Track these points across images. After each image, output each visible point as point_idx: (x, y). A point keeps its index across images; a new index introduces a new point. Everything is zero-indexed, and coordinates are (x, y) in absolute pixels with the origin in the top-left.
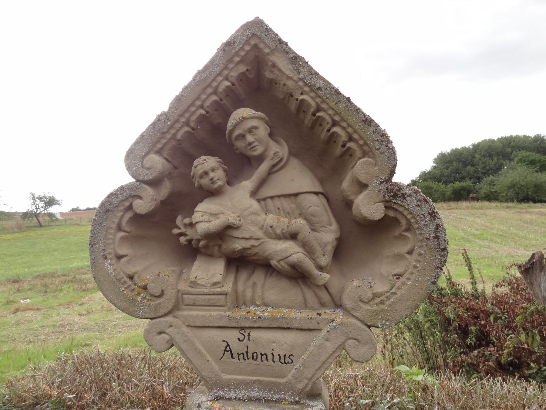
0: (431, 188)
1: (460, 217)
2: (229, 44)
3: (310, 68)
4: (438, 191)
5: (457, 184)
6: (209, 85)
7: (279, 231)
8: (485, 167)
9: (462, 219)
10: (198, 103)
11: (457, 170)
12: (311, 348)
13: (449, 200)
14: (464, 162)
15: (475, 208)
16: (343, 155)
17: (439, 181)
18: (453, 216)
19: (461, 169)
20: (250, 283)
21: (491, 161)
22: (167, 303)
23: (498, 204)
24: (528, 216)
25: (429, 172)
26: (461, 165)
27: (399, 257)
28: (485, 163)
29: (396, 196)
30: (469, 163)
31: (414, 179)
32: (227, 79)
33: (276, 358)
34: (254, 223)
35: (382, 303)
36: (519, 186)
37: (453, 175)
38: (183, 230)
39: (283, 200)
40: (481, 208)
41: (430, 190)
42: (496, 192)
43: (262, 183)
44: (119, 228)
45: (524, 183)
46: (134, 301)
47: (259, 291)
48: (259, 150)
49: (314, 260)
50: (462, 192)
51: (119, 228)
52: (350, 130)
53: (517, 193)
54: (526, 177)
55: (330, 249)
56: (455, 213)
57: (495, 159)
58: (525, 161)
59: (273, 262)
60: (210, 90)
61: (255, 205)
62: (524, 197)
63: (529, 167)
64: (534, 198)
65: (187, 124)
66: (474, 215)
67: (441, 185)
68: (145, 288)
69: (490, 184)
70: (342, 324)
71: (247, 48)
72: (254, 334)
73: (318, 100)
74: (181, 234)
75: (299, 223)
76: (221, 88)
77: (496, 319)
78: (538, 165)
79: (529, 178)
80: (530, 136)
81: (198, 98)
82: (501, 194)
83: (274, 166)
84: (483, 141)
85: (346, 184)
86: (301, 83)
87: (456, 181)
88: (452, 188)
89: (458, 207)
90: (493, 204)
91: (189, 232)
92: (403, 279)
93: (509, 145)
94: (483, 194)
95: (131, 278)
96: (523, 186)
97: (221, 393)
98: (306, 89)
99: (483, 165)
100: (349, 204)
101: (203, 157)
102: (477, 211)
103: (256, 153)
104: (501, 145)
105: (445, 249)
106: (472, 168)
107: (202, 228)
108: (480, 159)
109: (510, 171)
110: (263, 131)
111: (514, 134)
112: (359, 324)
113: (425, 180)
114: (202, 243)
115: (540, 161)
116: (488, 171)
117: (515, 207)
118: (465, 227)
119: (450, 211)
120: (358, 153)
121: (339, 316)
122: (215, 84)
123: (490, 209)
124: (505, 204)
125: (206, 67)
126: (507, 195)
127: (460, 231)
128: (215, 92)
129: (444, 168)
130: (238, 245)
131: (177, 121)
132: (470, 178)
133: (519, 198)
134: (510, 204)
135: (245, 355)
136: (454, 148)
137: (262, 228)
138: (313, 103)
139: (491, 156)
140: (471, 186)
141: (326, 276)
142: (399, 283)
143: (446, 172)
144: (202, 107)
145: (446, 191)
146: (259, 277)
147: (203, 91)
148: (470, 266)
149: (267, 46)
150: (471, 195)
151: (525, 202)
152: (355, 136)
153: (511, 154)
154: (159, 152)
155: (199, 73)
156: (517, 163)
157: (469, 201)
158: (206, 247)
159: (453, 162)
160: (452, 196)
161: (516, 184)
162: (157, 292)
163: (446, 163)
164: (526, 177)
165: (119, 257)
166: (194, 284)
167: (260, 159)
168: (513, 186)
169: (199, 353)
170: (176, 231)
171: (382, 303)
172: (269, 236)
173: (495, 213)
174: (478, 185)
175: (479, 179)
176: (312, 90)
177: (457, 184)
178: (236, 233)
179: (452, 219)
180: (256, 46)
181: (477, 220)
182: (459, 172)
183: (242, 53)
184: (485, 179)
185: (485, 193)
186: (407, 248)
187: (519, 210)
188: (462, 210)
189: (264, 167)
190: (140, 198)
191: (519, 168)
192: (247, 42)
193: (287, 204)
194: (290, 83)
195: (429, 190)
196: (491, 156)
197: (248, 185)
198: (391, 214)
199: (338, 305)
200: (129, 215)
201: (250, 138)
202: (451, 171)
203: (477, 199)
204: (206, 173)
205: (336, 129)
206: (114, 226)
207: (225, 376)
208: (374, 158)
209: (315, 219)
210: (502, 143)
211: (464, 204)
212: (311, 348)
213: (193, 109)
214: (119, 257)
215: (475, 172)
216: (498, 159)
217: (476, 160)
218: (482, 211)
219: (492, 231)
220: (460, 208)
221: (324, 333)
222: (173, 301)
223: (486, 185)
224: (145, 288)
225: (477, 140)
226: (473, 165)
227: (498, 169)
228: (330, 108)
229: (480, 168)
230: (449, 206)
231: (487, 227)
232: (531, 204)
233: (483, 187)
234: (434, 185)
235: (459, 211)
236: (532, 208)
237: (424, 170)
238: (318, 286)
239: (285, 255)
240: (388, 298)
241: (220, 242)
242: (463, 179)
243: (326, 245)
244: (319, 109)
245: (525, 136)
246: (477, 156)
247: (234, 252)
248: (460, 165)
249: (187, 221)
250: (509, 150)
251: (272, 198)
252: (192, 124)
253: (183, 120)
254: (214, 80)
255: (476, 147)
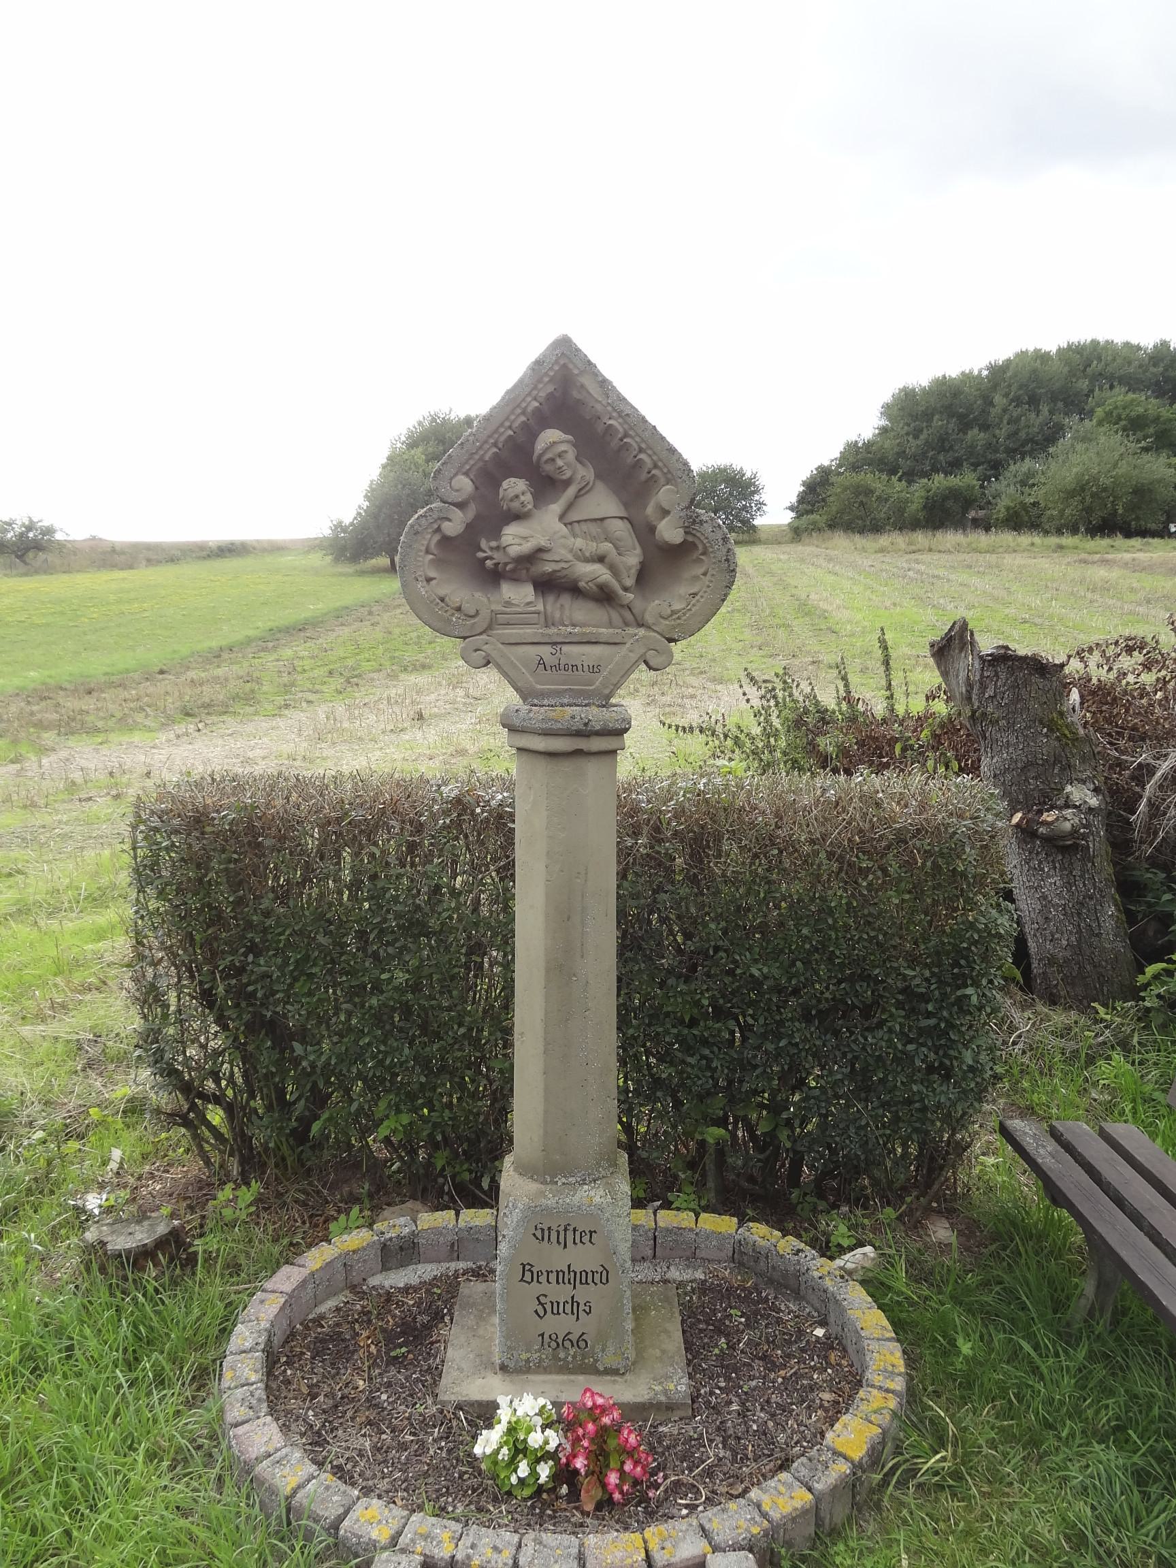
0: (869, 492)
1: (936, 573)
2: (538, 363)
3: (619, 395)
4: (887, 500)
5: (940, 481)
6: (518, 406)
7: (588, 554)
8: (1016, 433)
9: (938, 577)
10: (507, 424)
11: (942, 440)
12: (617, 659)
13: (914, 525)
14: (961, 417)
15: (976, 550)
16: (647, 481)
17: (893, 472)
18: (918, 572)
19: (954, 437)
20: (558, 605)
21: (1033, 415)
22: (481, 622)
23: (1037, 540)
24: (1101, 573)
25: (868, 445)
26: (953, 425)
27: (696, 578)
28: (1018, 420)
29: (694, 522)
30: (975, 419)
31: (826, 463)
32: (535, 399)
33: (586, 668)
34: (564, 546)
35: (679, 618)
36: (1094, 489)
37: (931, 454)
38: (489, 553)
39: (590, 524)
40: (992, 550)
41: (866, 495)
42: (1034, 504)
43: (570, 506)
44: (428, 552)
45: (1108, 482)
46: (449, 621)
47: (567, 613)
48: (568, 474)
49: (619, 582)
50: (949, 504)
51: (428, 552)
52: (655, 458)
53: (1089, 510)
54: (1115, 466)
55: (634, 572)
56: (924, 563)
57: (1045, 409)
58: (1120, 419)
59: (582, 584)
60: (519, 411)
61: (565, 530)
62: (1103, 519)
63: (1128, 436)
64: (1130, 525)
65: (495, 445)
66: (970, 567)
67: (897, 484)
68: (459, 609)
69: (1023, 483)
70: (644, 637)
71: (556, 368)
72: (565, 648)
73: (626, 426)
74: (487, 558)
75: (607, 547)
76: (530, 409)
77: (904, 750)
78: (1151, 430)
79: (1123, 468)
80: (1142, 345)
81: (507, 419)
82: (1049, 512)
83: (580, 490)
84: (1017, 355)
85: (650, 510)
86: (609, 408)
87: (937, 471)
88: (923, 494)
89: (933, 547)
90: (1025, 539)
91: (496, 555)
92: (698, 597)
93: (1084, 370)
94: (1003, 510)
95: (442, 600)
96: (1105, 490)
97: (536, 701)
98: (615, 414)
99: (1013, 428)
100: (652, 529)
101: (513, 480)
102: (981, 557)
103: (564, 477)
104: (1066, 370)
105: (734, 570)
106: (982, 434)
107: (514, 551)
108: (1005, 411)
109: (1080, 447)
110: (571, 455)
111: (1102, 338)
112: (659, 637)
113: (855, 468)
114: (508, 568)
115: (1157, 419)
116: (1023, 445)
117: (1076, 548)
118: (942, 601)
119: (913, 556)
120: (662, 481)
121: (642, 632)
122: (524, 405)
123: (1015, 551)
124: (1053, 540)
125: (515, 387)
126: (1062, 512)
127: (929, 611)
128: (524, 413)
129: (908, 434)
130: (549, 568)
131: (486, 442)
132: (975, 466)
133: (1090, 522)
134: (1068, 540)
135: (557, 667)
136: (939, 374)
137: (571, 551)
138: (621, 430)
139: (1033, 401)
140: (974, 486)
141: (630, 596)
142: (694, 601)
143: (913, 445)
144: (510, 427)
145: (907, 501)
146: (566, 599)
147: (512, 412)
148: (888, 664)
149: (576, 366)
150: (972, 514)
151: (1102, 537)
152: (660, 464)
153: (1088, 396)
154: (466, 474)
155: (508, 392)
156: (1100, 423)
157: (964, 530)
158: (513, 571)
159: (933, 415)
160: (921, 515)
161: (1088, 482)
162: (472, 612)
163: (915, 417)
164: (1115, 466)
165: (429, 580)
166: (508, 604)
167: (567, 483)
168: (1079, 490)
169: (515, 666)
170: (481, 555)
171: (679, 618)
172: (578, 559)
173: (1023, 562)
174: (995, 486)
175: (996, 468)
176: (620, 416)
177: (940, 481)
178: (546, 556)
179: (912, 579)
180: (565, 366)
181: (975, 580)
182: (947, 445)
183: (552, 373)
184: (1012, 468)
185: (1008, 508)
186: (702, 570)
187: (1084, 556)
188: (942, 555)
189: (571, 491)
190: (450, 520)
191: (1102, 439)
192: (556, 362)
193: (594, 529)
194: (598, 407)
195: (861, 498)
196: (1034, 401)
197: (556, 508)
198: (690, 539)
199: (640, 625)
200: (437, 537)
201: (560, 462)
202: (927, 441)
203: (986, 525)
204: (517, 497)
205: (642, 456)
206: (423, 548)
207: (539, 687)
208: (676, 486)
209: (621, 544)
210: (1068, 362)
211: (950, 538)
212: (617, 659)
213: (502, 430)
214: (429, 580)
215: (989, 446)
216: (1051, 412)
217: (994, 411)
218: (992, 558)
219: (1007, 611)
220: (941, 548)
221: (628, 645)
222: (488, 620)
223: (1012, 487)
224: (459, 609)
225: (1002, 351)
226: (985, 427)
227: (1052, 435)
228: (637, 435)
229: (1002, 433)
230: (910, 544)
231: (996, 599)
232: (1119, 541)
233: (1005, 492)
234: (876, 481)
235: (936, 556)
236: (1118, 550)
237: (853, 438)
238: (622, 606)
239: (593, 576)
240: (684, 614)
241: (528, 565)
242: (954, 466)
243: (630, 568)
244: (626, 435)
245: (1127, 345)
246: (999, 399)
247: (544, 574)
248: (951, 426)
249: (494, 544)
250: (1084, 384)
251: (578, 522)
252: (500, 445)
253: (492, 441)
254: (524, 400)
255: (998, 372)
